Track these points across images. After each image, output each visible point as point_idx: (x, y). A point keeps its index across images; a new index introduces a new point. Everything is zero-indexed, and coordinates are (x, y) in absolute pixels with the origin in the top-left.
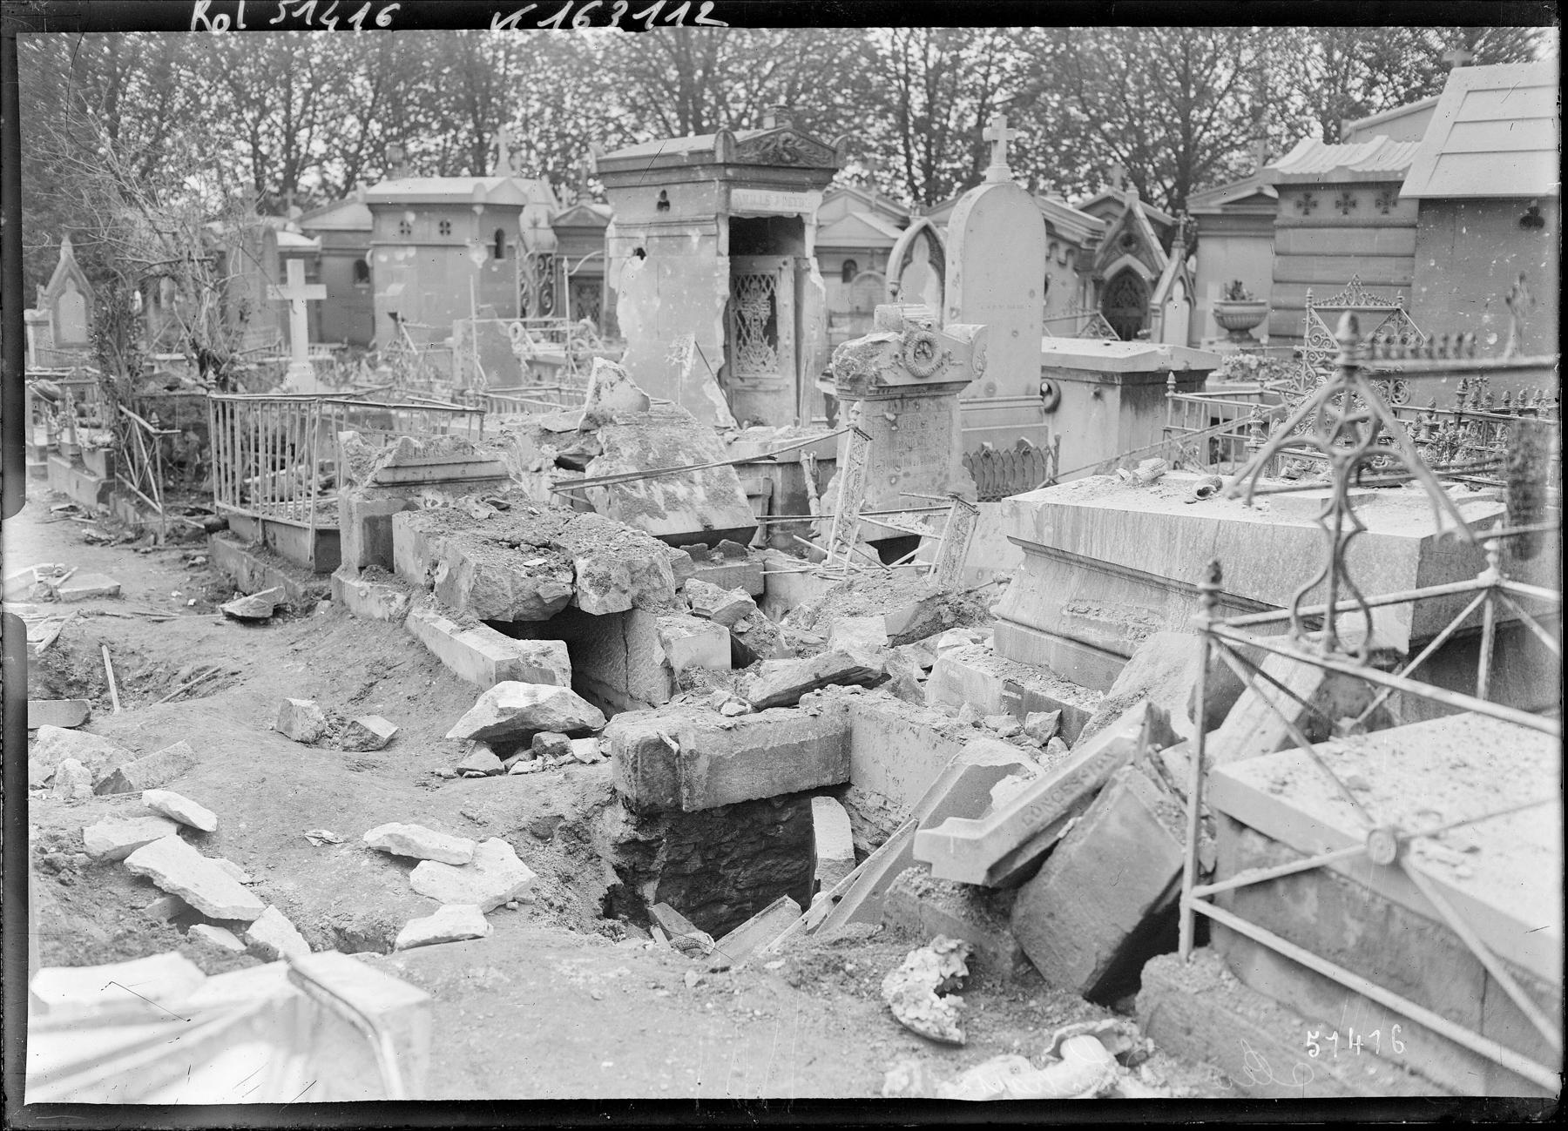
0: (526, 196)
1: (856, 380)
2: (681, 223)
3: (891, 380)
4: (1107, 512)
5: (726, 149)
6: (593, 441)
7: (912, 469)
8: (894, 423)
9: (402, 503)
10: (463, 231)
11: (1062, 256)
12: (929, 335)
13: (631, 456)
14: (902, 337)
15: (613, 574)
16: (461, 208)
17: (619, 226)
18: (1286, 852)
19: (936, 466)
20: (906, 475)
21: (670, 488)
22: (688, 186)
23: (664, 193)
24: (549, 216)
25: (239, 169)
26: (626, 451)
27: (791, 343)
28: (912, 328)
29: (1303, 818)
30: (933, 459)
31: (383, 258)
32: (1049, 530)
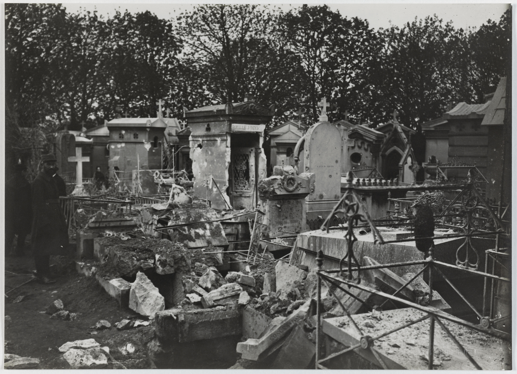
0: (166, 125)
1: (266, 192)
2: (215, 136)
3: (278, 192)
4: (329, 239)
5: (229, 110)
6: (171, 213)
7: (287, 225)
8: (280, 208)
9: (97, 235)
10: (143, 137)
11: (366, 147)
12: (293, 176)
13: (184, 219)
14: (282, 178)
15: (168, 260)
16: (141, 129)
17: (193, 136)
18: (342, 347)
19: (297, 224)
20: (285, 227)
21: (197, 231)
22: (217, 123)
23: (208, 125)
24: (176, 131)
25: (65, 113)
26: (182, 217)
27: (254, 179)
28: (287, 174)
29: (347, 335)
30: (295, 221)
31: (113, 147)
32: (312, 245)
